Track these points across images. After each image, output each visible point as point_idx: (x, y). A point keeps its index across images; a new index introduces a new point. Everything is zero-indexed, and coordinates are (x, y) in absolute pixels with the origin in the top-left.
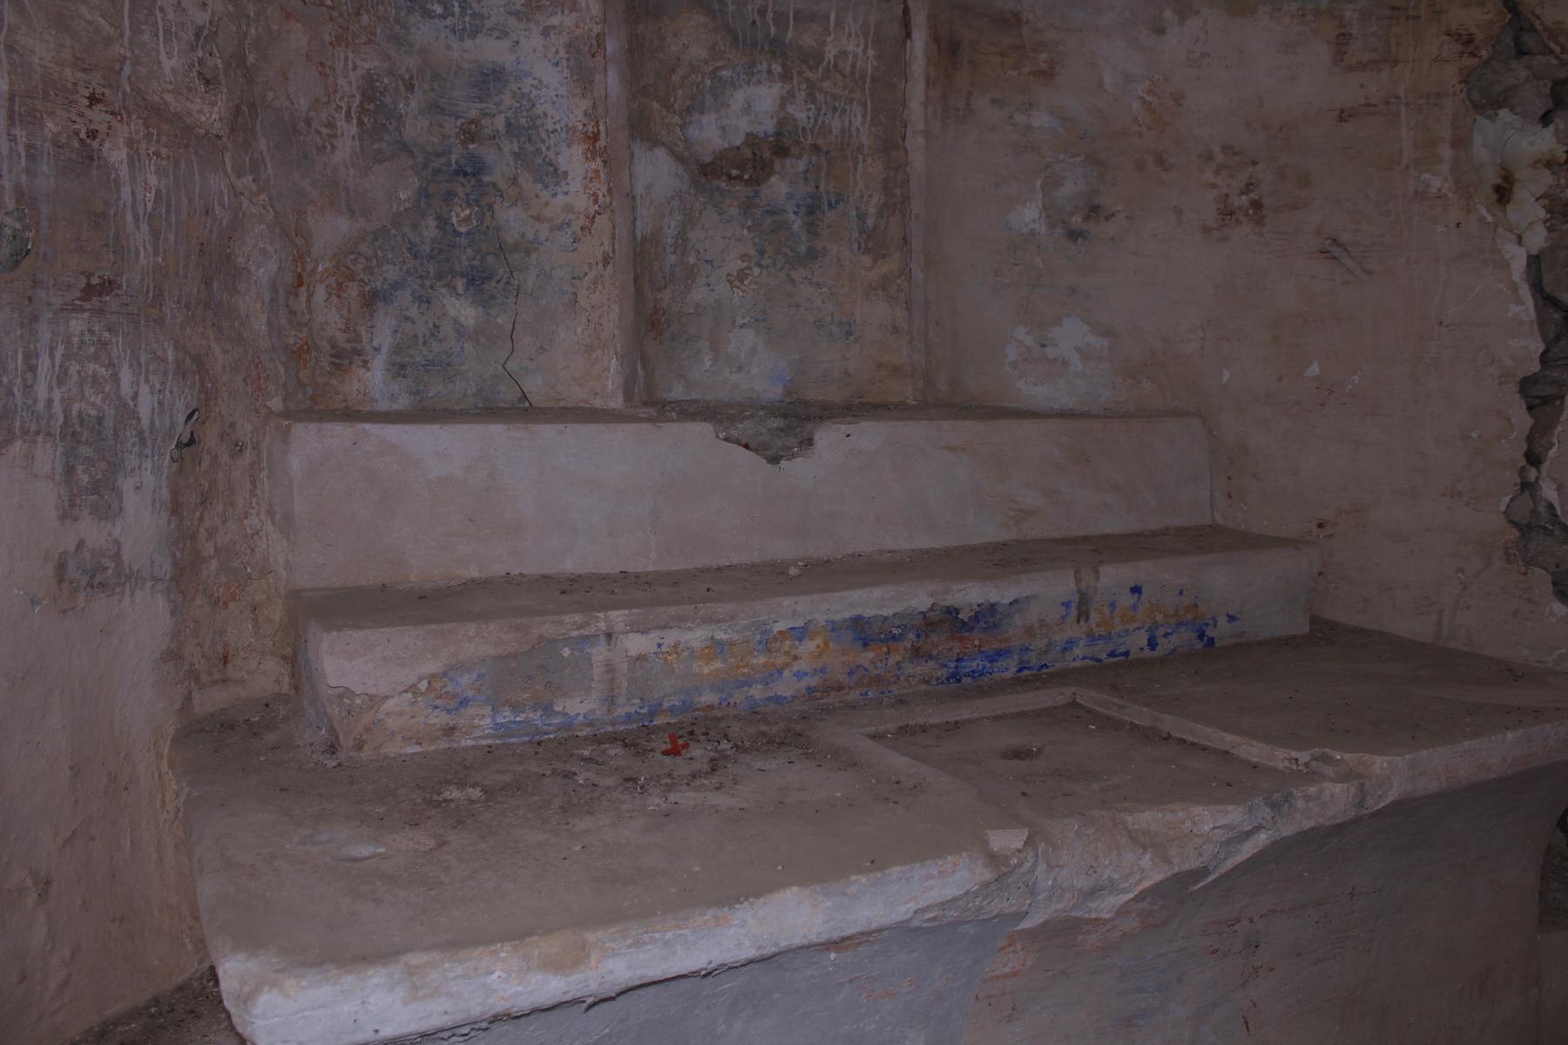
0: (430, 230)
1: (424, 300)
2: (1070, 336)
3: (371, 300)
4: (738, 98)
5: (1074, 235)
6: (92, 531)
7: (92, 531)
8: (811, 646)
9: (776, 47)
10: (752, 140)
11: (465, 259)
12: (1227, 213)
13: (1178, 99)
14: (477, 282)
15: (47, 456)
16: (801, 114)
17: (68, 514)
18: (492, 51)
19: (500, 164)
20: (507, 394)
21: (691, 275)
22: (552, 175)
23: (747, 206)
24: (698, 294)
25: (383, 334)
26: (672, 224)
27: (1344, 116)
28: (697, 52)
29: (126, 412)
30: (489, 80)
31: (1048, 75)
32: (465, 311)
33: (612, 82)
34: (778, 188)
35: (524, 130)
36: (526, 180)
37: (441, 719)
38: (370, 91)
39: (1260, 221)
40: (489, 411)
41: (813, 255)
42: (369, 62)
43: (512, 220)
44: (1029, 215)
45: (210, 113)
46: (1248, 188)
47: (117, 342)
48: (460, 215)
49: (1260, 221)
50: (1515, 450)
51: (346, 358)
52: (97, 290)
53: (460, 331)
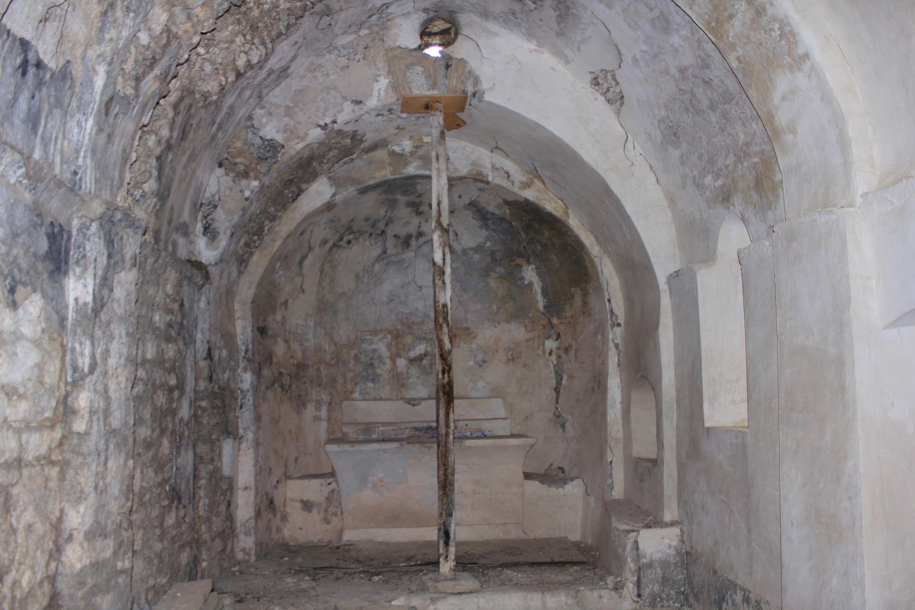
0: (365, 374)
1: (364, 384)
2: (481, 384)
3: (356, 384)
4: (417, 348)
5: (480, 366)
6: (318, 413)
7: (318, 413)
8: (408, 431)
9: (425, 338)
10: (420, 355)
11: (371, 377)
12: (508, 360)
13: (500, 339)
14: (373, 381)
15: (313, 404)
16: (429, 349)
17: (315, 411)
18: (374, 346)
19: (376, 363)
20: (379, 397)
21: (409, 378)
22: (384, 364)
23: (419, 365)
24: (411, 380)
25: (358, 389)
26: (405, 370)
27: (527, 340)
28: (410, 341)
29: (322, 399)
30: (375, 351)
31: (475, 337)
32: (371, 385)
33: (393, 349)
34: (425, 362)
35: (380, 358)
36: (381, 366)
37: (356, 436)
38: (356, 355)
39: (513, 361)
40: (375, 400)
41: (431, 373)
42: (355, 351)
43: (379, 371)
44: (471, 363)
45: (333, 362)
46: (512, 355)
47: (134, 107)
48: (370, 371)
49: (513, 361)
50: (553, 401)
51: (352, 392)
52: (319, 385)
53: (370, 388)
